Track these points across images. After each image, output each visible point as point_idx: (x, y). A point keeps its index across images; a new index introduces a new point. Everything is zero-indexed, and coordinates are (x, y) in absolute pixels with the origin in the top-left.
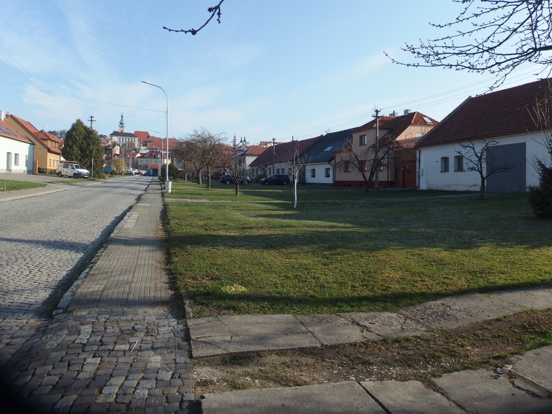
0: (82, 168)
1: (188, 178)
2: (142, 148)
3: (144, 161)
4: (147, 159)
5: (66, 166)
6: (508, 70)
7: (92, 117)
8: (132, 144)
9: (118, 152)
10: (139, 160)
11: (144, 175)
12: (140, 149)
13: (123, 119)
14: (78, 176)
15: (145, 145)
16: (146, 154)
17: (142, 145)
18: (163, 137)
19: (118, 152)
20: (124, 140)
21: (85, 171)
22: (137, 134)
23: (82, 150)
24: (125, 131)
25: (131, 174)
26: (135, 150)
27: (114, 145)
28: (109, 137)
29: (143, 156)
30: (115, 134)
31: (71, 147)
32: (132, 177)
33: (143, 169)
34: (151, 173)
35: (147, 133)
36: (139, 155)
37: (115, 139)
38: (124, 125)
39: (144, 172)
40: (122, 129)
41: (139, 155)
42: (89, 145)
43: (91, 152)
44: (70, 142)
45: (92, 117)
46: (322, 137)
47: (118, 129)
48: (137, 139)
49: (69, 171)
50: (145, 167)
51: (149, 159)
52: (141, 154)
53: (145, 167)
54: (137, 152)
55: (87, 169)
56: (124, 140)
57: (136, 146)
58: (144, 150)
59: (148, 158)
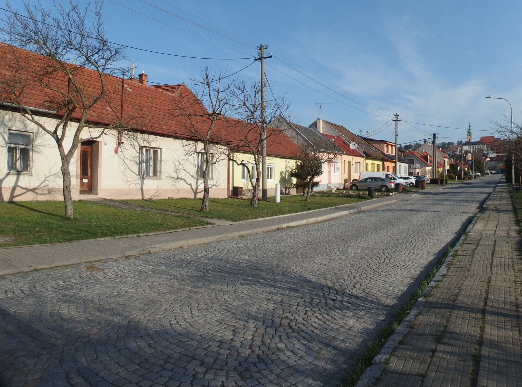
1: (399, 159)
6: (254, 180)
8: (481, 150)
9: (470, 158)
11: (494, 174)
13: (471, 128)
15: (492, 150)
16: (494, 158)
18: (70, 170)
19: (470, 158)
21: (480, 174)
22: (483, 141)
26: (484, 154)
27: (467, 152)
29: (492, 159)
34: (500, 172)
36: (488, 159)
37: (466, 148)
38: (472, 133)
39: (494, 172)
41: (488, 159)
46: (280, 158)
52: (490, 158)
54: (487, 157)
59: (496, 160)
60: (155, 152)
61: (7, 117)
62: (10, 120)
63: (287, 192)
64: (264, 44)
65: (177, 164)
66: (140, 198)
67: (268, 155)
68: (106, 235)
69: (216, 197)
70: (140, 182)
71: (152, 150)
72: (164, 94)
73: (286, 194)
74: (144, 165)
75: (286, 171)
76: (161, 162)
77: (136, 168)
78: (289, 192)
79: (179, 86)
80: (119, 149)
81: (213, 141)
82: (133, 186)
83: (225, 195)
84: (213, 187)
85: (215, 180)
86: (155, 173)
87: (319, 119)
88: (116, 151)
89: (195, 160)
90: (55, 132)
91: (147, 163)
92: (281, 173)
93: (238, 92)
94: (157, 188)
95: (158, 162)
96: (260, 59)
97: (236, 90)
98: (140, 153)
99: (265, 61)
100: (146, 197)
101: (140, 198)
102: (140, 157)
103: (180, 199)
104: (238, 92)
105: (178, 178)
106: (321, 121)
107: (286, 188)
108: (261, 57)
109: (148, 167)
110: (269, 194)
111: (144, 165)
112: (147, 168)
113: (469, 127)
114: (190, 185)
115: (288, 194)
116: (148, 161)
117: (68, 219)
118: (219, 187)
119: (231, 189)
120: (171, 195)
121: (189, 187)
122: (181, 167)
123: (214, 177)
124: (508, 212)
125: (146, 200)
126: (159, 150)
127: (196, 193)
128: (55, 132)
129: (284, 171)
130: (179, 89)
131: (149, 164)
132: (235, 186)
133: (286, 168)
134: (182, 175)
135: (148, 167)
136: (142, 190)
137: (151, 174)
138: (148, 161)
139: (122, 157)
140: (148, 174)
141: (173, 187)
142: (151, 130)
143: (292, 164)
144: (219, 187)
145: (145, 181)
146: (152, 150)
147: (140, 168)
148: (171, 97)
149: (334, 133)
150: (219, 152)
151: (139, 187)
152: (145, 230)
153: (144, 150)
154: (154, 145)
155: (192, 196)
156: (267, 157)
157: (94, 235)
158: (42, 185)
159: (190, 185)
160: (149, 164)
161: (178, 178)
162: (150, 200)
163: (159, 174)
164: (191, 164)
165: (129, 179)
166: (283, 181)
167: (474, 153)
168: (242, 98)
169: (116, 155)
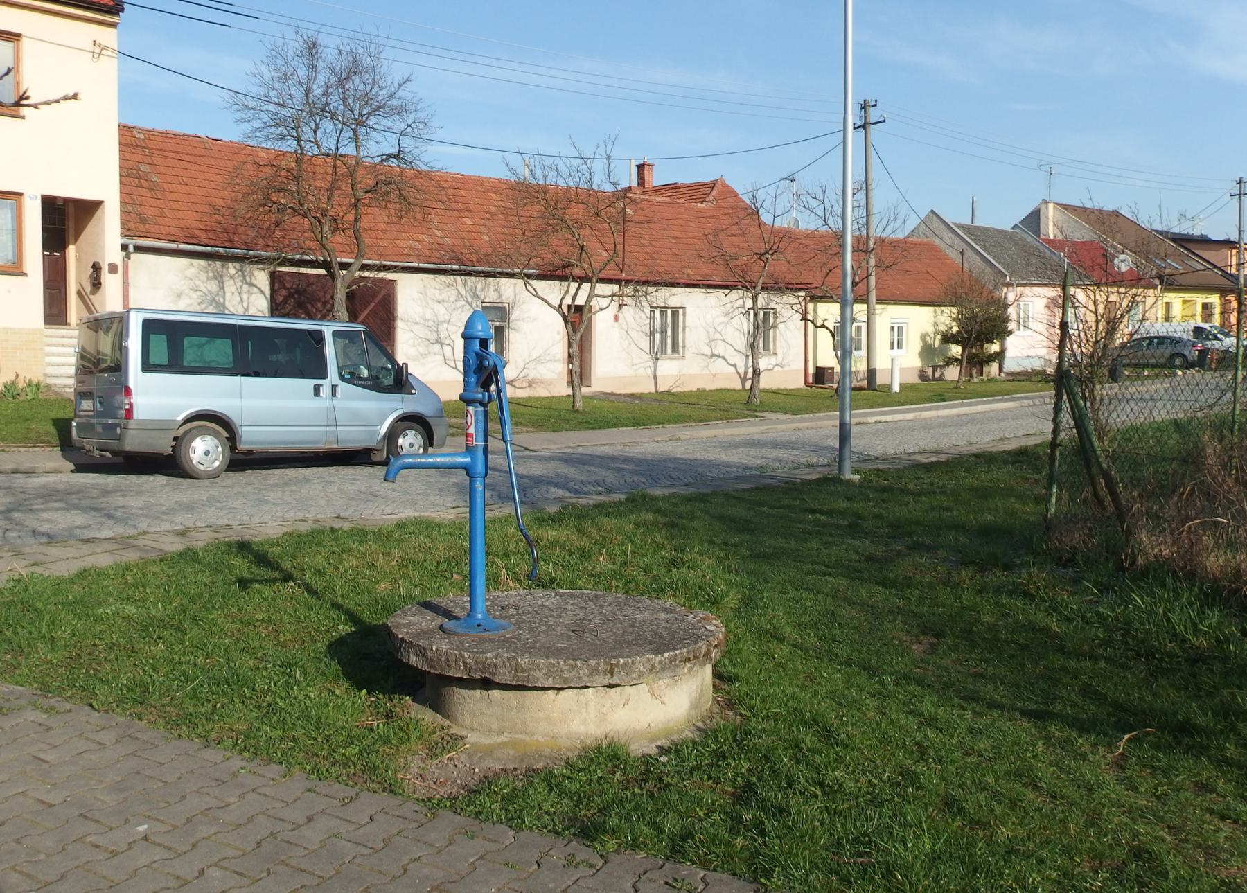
60: (675, 314)
61: (479, 286)
62: (483, 289)
63: (937, 375)
64: (871, 98)
65: (711, 331)
66: (653, 390)
67: (880, 301)
68: (627, 426)
69: (782, 387)
70: (651, 365)
71: (669, 311)
72: (686, 209)
73: (934, 379)
74: (657, 336)
75: (936, 333)
76: (684, 329)
77: (645, 343)
78: (942, 374)
79: (713, 185)
80: (620, 315)
81: (777, 286)
82: (641, 371)
83: (801, 384)
84: (777, 368)
85: (780, 357)
86: (675, 349)
87: (1045, 202)
88: (616, 318)
89: (743, 324)
90: (560, 306)
91: (661, 333)
92: (923, 337)
93: (813, 203)
94: (682, 373)
95: (680, 330)
96: (864, 126)
97: (810, 200)
98: (652, 317)
99: (872, 129)
100: (661, 389)
101: (653, 390)
102: (652, 325)
103: (717, 390)
104: (813, 203)
105: (713, 355)
106: (1051, 206)
107: (935, 368)
108: (865, 123)
109: (663, 340)
110: (881, 380)
111: (657, 336)
112: (661, 341)
114: (735, 366)
115: (941, 378)
116: (663, 330)
117: (577, 411)
118: (787, 368)
119: (811, 371)
120: (701, 386)
121: (733, 369)
122: (718, 336)
123: (778, 351)
125: (662, 393)
126: (681, 311)
127: (743, 381)
128: (560, 306)
129: (931, 330)
130: (714, 193)
131: (667, 335)
132: (819, 365)
133: (936, 324)
134: (720, 349)
135: (663, 340)
136: (655, 377)
137: (669, 351)
138: (663, 330)
139: (625, 327)
140: (664, 351)
141: (706, 372)
142: (668, 278)
143: (946, 318)
144: (787, 368)
145: (660, 363)
146: (669, 311)
147: (652, 342)
148: (700, 210)
149: (1082, 233)
150: (786, 307)
151: (650, 372)
152: (669, 422)
153: (657, 312)
154: (673, 302)
155: (739, 386)
156: (878, 306)
157: (615, 425)
159: (735, 366)
160: (667, 335)
161: (713, 355)
162: (668, 393)
163: (681, 349)
164: (737, 331)
165: (635, 361)
166: (927, 351)
168: (821, 214)
169: (616, 324)
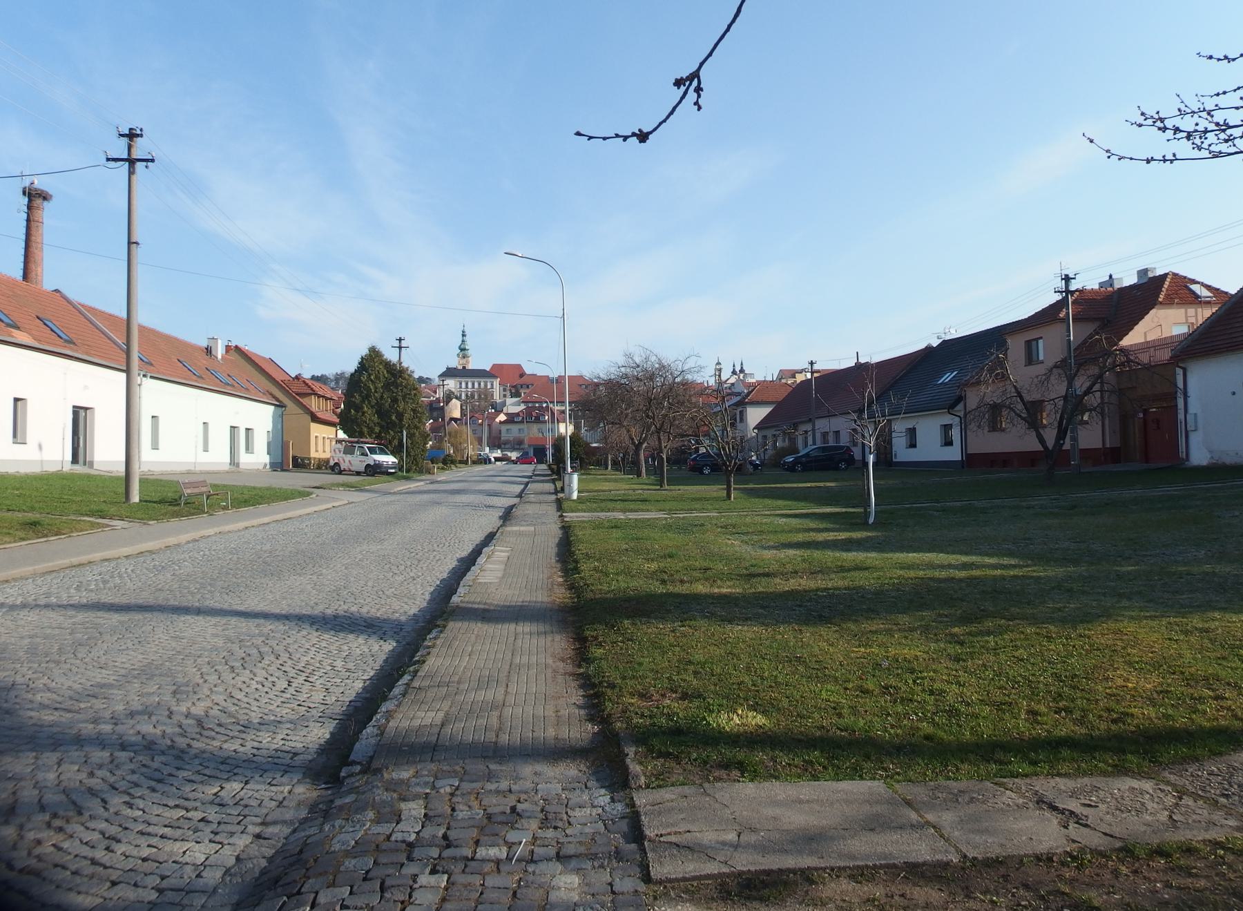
0: (383, 452)
2: (510, 401)
3: (514, 431)
4: (521, 426)
5: (349, 450)
7: (400, 340)
8: (486, 395)
10: (504, 428)
11: (515, 462)
12: (504, 404)
13: (466, 339)
14: (374, 470)
15: (516, 394)
16: (518, 414)
17: (508, 393)
20: (470, 385)
21: (389, 459)
22: (497, 371)
23: (381, 413)
24: (470, 367)
25: (486, 461)
26: (494, 406)
27: (449, 397)
28: (437, 381)
29: (511, 419)
30: (450, 373)
31: (358, 408)
32: (488, 467)
33: (513, 449)
35: (519, 367)
36: (502, 417)
37: (451, 384)
38: (469, 353)
39: (514, 455)
40: (464, 361)
41: (502, 417)
42: (395, 400)
43: (400, 416)
44: (357, 398)
45: (400, 340)
47: (455, 363)
48: (496, 382)
49: (356, 461)
50: (517, 444)
51: (524, 426)
52: (506, 414)
53: (517, 444)
54: (499, 412)
55: (393, 453)
56: (470, 385)
57: (497, 397)
58: (514, 406)
59: (522, 422)
101: (712, 382)
113: (464, 335)
124: (761, 571)
158: (1194, 287)
167: (467, 401)
